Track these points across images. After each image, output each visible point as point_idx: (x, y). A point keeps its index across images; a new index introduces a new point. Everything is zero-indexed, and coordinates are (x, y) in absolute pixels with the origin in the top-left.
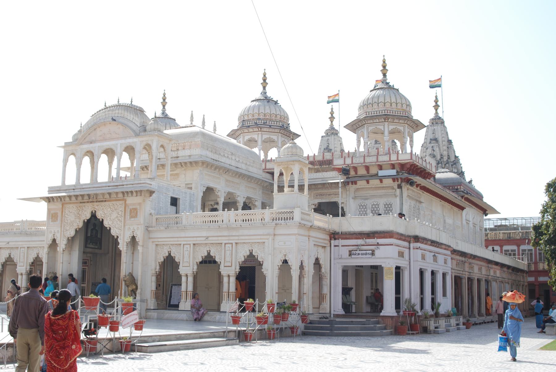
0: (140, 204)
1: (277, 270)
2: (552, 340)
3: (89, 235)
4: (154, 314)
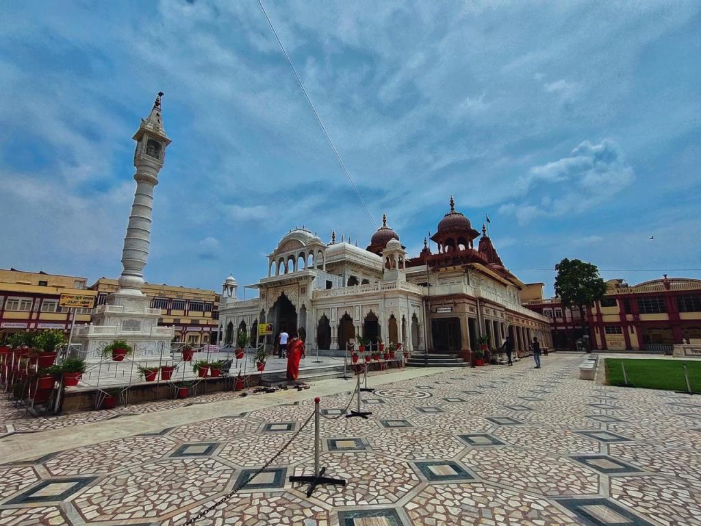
2: (457, 474)
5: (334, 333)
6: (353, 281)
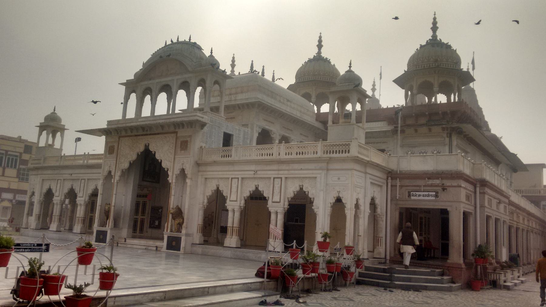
0: (190, 136)
1: (330, 208)
3: (147, 169)
4: (199, 249)
5: (233, 220)
6: (265, 138)
